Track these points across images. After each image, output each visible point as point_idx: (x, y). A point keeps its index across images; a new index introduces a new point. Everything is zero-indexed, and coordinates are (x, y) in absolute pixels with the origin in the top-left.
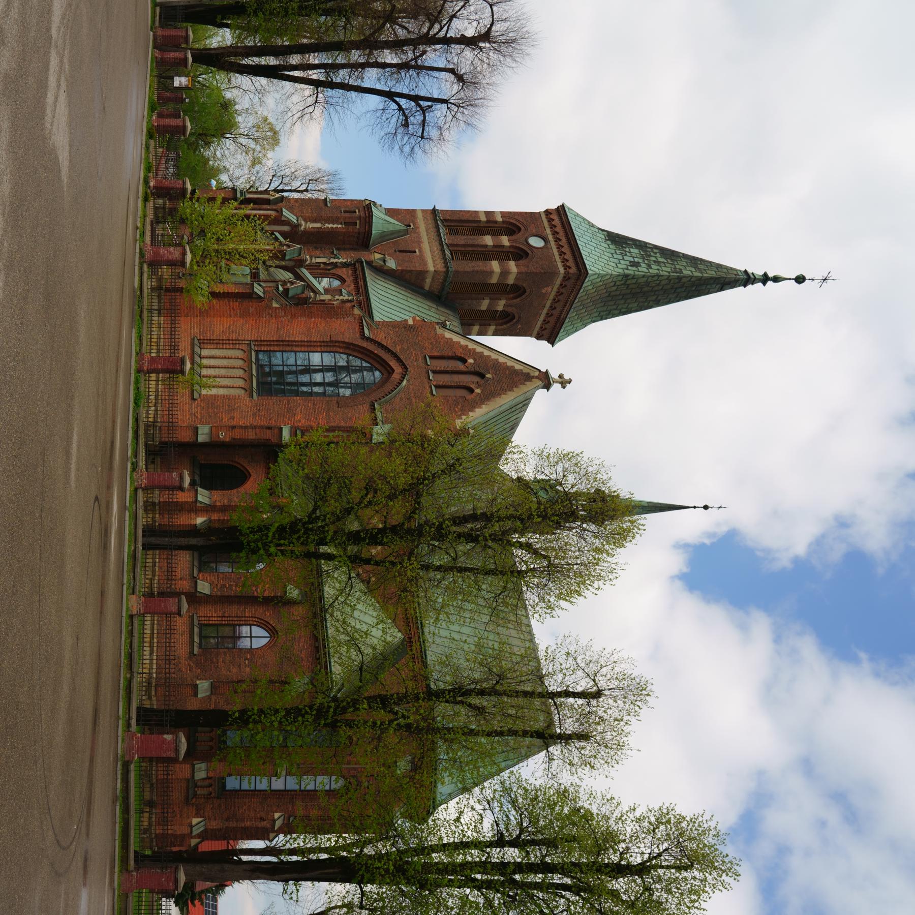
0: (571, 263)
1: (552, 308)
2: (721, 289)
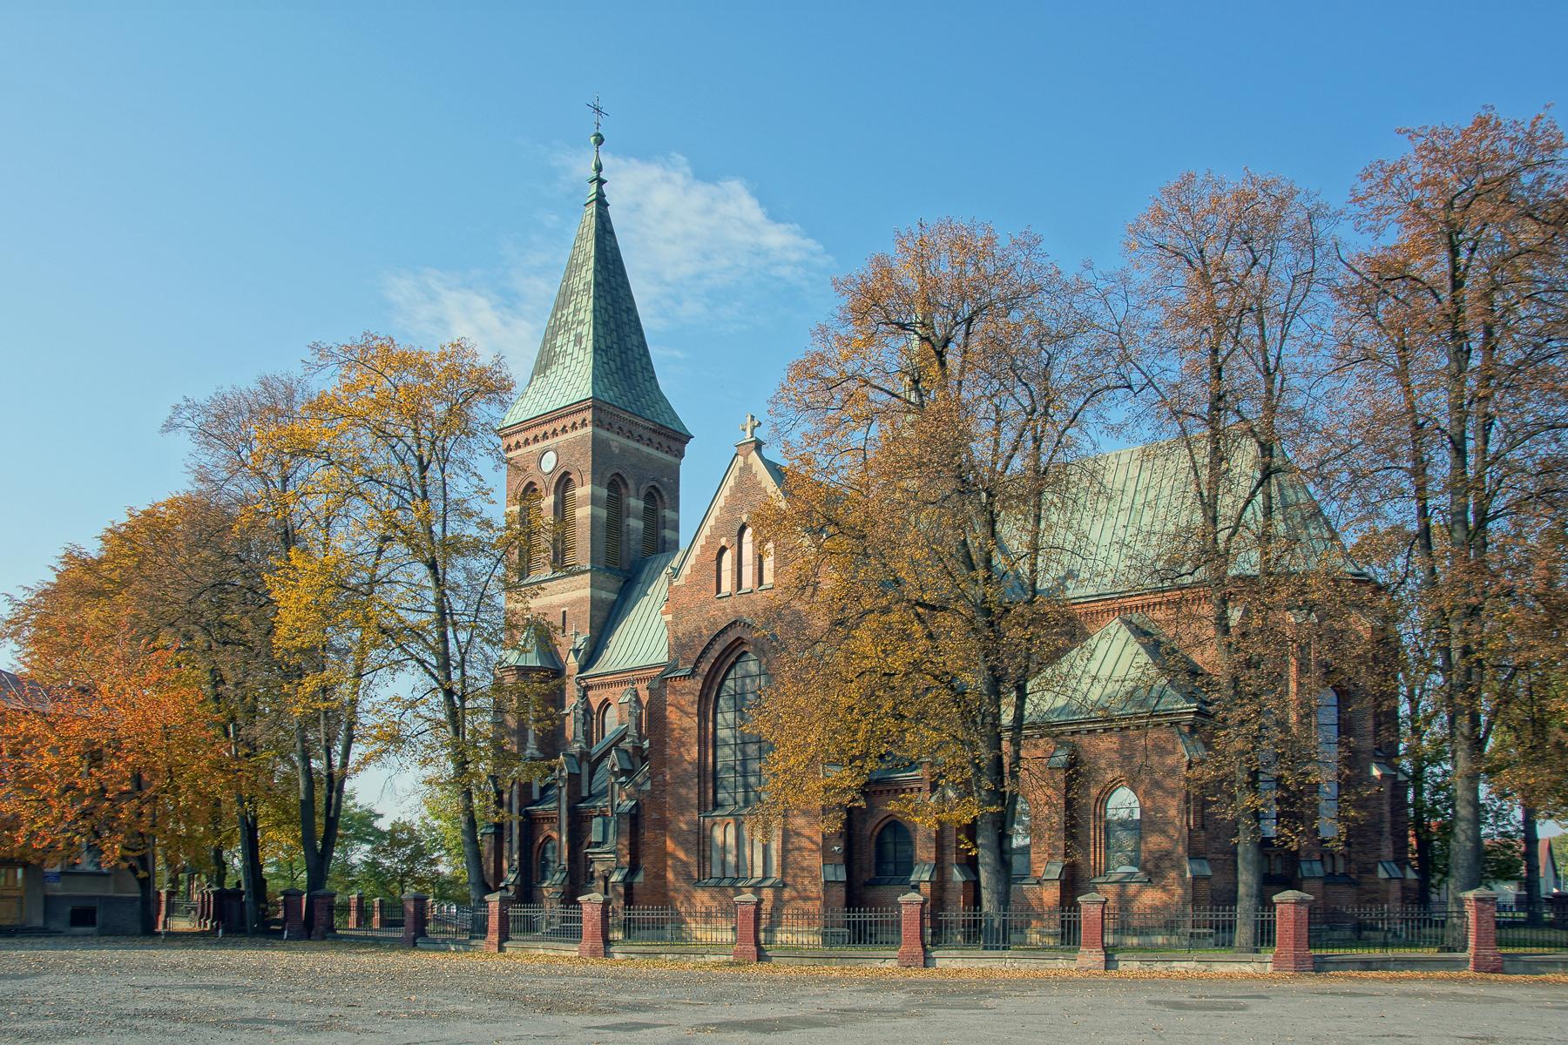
0: (578, 418)
1: (640, 439)
2: (612, 233)
